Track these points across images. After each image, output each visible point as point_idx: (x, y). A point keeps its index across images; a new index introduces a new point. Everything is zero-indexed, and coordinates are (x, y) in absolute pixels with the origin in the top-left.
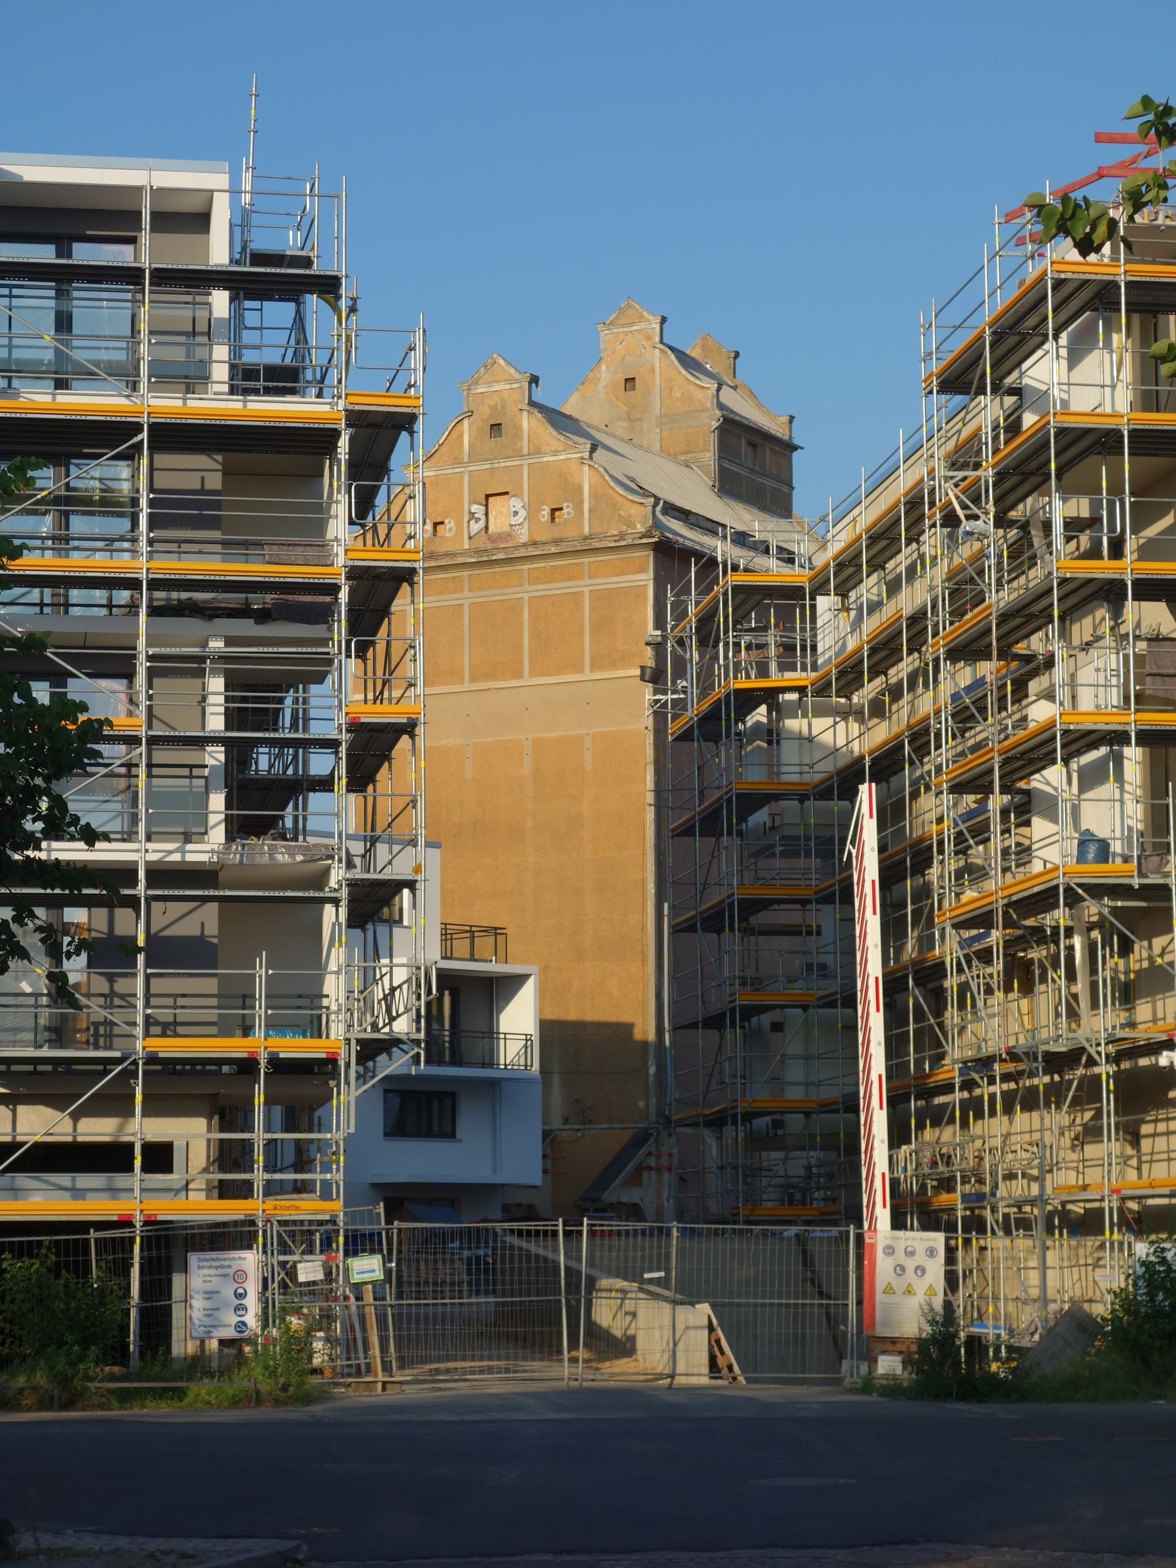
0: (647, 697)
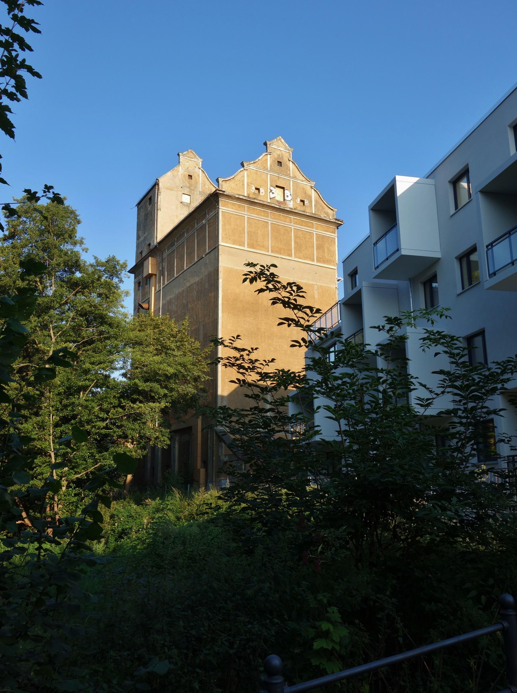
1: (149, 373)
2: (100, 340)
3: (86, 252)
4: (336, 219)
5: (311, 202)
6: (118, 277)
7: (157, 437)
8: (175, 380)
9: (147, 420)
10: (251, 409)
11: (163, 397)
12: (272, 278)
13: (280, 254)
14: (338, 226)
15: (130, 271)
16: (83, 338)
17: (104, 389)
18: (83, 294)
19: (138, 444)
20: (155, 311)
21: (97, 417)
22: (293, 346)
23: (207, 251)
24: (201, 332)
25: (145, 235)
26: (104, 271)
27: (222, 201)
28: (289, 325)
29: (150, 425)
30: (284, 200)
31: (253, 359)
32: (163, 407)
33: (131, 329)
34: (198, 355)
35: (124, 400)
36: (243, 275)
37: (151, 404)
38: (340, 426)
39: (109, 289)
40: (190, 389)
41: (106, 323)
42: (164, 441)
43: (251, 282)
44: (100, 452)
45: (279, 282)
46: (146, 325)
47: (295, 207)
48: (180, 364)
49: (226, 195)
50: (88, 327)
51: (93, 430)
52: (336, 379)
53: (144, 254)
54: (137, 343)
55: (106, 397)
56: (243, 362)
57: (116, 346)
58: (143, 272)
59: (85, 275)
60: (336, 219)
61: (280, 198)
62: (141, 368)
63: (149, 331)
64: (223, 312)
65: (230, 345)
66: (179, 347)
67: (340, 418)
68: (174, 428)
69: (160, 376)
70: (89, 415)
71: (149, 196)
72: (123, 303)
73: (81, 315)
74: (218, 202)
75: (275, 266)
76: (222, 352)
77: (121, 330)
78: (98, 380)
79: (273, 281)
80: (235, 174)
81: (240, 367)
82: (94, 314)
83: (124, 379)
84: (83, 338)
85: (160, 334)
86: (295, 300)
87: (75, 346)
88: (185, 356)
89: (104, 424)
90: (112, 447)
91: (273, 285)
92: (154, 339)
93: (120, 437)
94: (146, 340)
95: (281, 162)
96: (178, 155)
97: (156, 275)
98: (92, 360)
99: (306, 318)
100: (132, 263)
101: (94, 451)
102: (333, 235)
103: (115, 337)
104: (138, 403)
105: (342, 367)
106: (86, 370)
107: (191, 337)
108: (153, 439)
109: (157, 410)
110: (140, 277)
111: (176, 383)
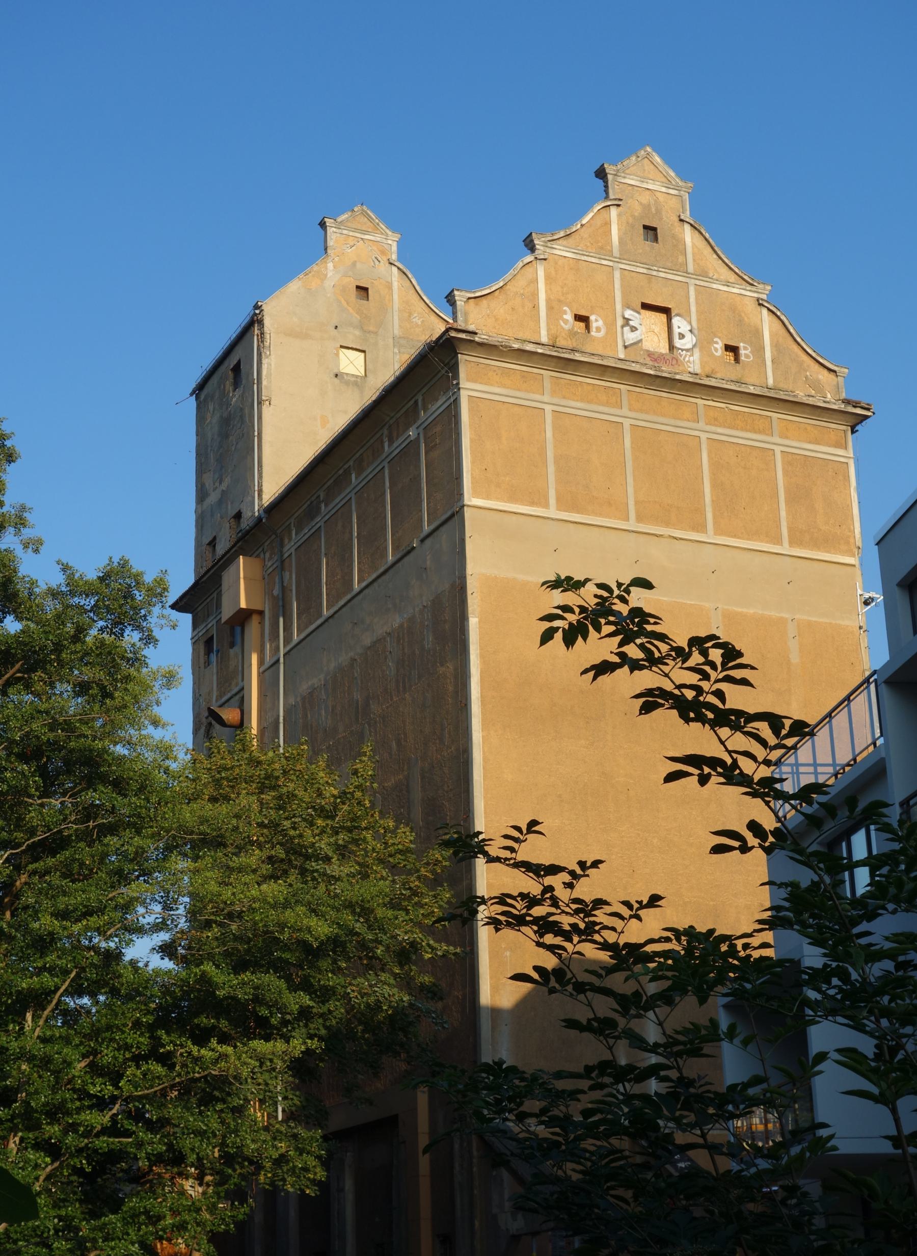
0: (860, 592)
1: (250, 940)
2: (86, 836)
3: (36, 551)
4: (847, 402)
5: (759, 350)
6: (139, 628)
7: (282, 1156)
8: (335, 962)
9: (247, 1100)
10: (589, 1069)
11: (298, 1019)
12: (639, 625)
13: (667, 524)
14: (856, 422)
15: (178, 606)
16: (32, 832)
17: (102, 998)
18: (28, 687)
19: (217, 1184)
20: (262, 730)
21: (82, 1094)
22: (718, 849)
23: (426, 528)
24: (417, 795)
25: (224, 486)
26: (95, 608)
27: (467, 364)
28: (703, 780)
29: (259, 1115)
30: (672, 347)
31: (588, 899)
32: (297, 1054)
33: (185, 796)
34: (409, 873)
35: (168, 1033)
36: (542, 619)
37: (258, 1045)
38: (897, 1121)
39: (112, 668)
40: (387, 990)
41: (103, 779)
42: (306, 1169)
43: (569, 641)
44: (94, 1215)
45: (662, 637)
46: (234, 782)
47: (708, 370)
48: (350, 906)
49: (481, 345)
50: (46, 794)
51: (70, 1139)
52: (874, 956)
53: (221, 549)
54: (207, 842)
55: (109, 1028)
56: (553, 910)
57: (139, 855)
58: (219, 605)
59: (32, 625)
60: (847, 402)
61: (656, 343)
62: (221, 925)
63: (246, 800)
64: (485, 726)
65: (507, 854)
66: (345, 847)
67: (898, 1095)
68: (339, 1121)
69: (286, 948)
70: (54, 1089)
71: (232, 361)
72: (156, 710)
73: (23, 758)
74: (454, 368)
75: (646, 584)
76: (487, 879)
77: (154, 799)
78: (83, 969)
79: (642, 632)
80: (508, 276)
81: (545, 926)
82: (63, 752)
83: (168, 964)
84: (32, 832)
85: (280, 808)
86: (720, 694)
87: (7, 860)
88: (365, 876)
89: (106, 1119)
90: (132, 1195)
91: (642, 647)
92: (261, 825)
93: (158, 1159)
94: (236, 829)
95: (654, 229)
96: (323, 225)
97: (261, 613)
98: (62, 902)
99: (760, 752)
100: (182, 579)
101: (73, 1210)
102: (841, 452)
103: (134, 825)
104: (214, 1042)
105: (894, 912)
106: (41, 938)
107: (382, 815)
108: (268, 1165)
109: (279, 1064)
110: (212, 623)
111: (340, 968)
